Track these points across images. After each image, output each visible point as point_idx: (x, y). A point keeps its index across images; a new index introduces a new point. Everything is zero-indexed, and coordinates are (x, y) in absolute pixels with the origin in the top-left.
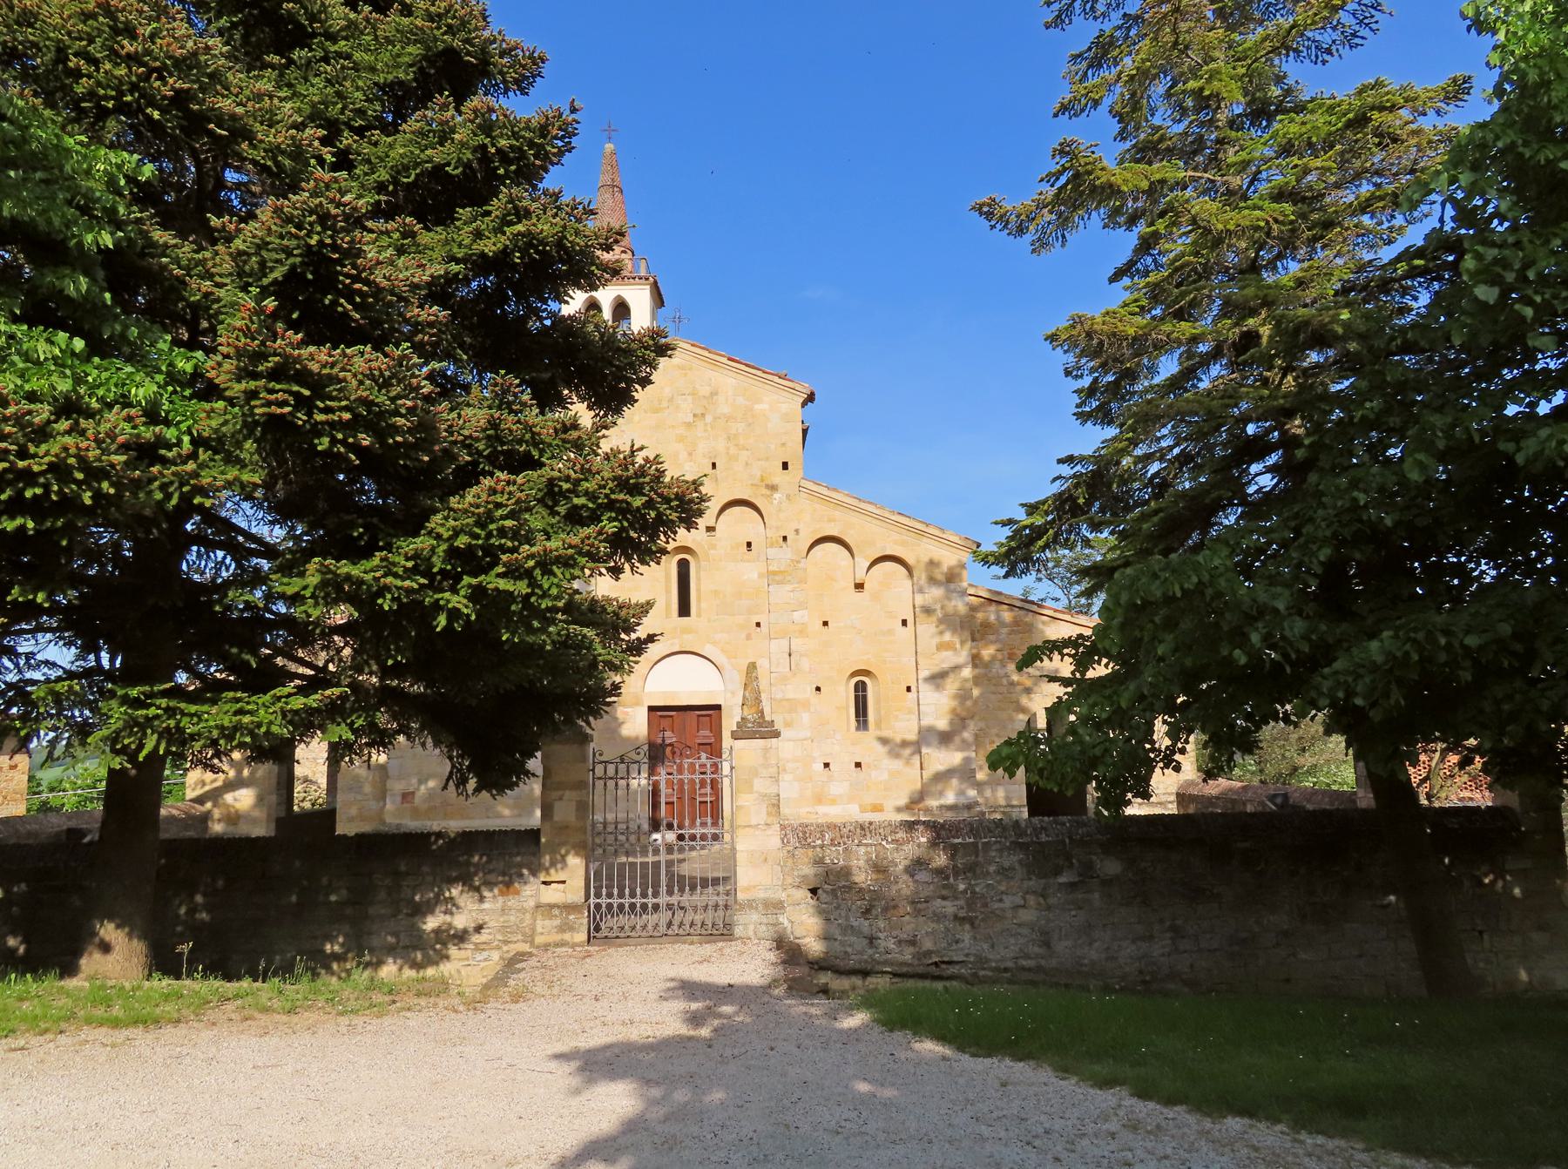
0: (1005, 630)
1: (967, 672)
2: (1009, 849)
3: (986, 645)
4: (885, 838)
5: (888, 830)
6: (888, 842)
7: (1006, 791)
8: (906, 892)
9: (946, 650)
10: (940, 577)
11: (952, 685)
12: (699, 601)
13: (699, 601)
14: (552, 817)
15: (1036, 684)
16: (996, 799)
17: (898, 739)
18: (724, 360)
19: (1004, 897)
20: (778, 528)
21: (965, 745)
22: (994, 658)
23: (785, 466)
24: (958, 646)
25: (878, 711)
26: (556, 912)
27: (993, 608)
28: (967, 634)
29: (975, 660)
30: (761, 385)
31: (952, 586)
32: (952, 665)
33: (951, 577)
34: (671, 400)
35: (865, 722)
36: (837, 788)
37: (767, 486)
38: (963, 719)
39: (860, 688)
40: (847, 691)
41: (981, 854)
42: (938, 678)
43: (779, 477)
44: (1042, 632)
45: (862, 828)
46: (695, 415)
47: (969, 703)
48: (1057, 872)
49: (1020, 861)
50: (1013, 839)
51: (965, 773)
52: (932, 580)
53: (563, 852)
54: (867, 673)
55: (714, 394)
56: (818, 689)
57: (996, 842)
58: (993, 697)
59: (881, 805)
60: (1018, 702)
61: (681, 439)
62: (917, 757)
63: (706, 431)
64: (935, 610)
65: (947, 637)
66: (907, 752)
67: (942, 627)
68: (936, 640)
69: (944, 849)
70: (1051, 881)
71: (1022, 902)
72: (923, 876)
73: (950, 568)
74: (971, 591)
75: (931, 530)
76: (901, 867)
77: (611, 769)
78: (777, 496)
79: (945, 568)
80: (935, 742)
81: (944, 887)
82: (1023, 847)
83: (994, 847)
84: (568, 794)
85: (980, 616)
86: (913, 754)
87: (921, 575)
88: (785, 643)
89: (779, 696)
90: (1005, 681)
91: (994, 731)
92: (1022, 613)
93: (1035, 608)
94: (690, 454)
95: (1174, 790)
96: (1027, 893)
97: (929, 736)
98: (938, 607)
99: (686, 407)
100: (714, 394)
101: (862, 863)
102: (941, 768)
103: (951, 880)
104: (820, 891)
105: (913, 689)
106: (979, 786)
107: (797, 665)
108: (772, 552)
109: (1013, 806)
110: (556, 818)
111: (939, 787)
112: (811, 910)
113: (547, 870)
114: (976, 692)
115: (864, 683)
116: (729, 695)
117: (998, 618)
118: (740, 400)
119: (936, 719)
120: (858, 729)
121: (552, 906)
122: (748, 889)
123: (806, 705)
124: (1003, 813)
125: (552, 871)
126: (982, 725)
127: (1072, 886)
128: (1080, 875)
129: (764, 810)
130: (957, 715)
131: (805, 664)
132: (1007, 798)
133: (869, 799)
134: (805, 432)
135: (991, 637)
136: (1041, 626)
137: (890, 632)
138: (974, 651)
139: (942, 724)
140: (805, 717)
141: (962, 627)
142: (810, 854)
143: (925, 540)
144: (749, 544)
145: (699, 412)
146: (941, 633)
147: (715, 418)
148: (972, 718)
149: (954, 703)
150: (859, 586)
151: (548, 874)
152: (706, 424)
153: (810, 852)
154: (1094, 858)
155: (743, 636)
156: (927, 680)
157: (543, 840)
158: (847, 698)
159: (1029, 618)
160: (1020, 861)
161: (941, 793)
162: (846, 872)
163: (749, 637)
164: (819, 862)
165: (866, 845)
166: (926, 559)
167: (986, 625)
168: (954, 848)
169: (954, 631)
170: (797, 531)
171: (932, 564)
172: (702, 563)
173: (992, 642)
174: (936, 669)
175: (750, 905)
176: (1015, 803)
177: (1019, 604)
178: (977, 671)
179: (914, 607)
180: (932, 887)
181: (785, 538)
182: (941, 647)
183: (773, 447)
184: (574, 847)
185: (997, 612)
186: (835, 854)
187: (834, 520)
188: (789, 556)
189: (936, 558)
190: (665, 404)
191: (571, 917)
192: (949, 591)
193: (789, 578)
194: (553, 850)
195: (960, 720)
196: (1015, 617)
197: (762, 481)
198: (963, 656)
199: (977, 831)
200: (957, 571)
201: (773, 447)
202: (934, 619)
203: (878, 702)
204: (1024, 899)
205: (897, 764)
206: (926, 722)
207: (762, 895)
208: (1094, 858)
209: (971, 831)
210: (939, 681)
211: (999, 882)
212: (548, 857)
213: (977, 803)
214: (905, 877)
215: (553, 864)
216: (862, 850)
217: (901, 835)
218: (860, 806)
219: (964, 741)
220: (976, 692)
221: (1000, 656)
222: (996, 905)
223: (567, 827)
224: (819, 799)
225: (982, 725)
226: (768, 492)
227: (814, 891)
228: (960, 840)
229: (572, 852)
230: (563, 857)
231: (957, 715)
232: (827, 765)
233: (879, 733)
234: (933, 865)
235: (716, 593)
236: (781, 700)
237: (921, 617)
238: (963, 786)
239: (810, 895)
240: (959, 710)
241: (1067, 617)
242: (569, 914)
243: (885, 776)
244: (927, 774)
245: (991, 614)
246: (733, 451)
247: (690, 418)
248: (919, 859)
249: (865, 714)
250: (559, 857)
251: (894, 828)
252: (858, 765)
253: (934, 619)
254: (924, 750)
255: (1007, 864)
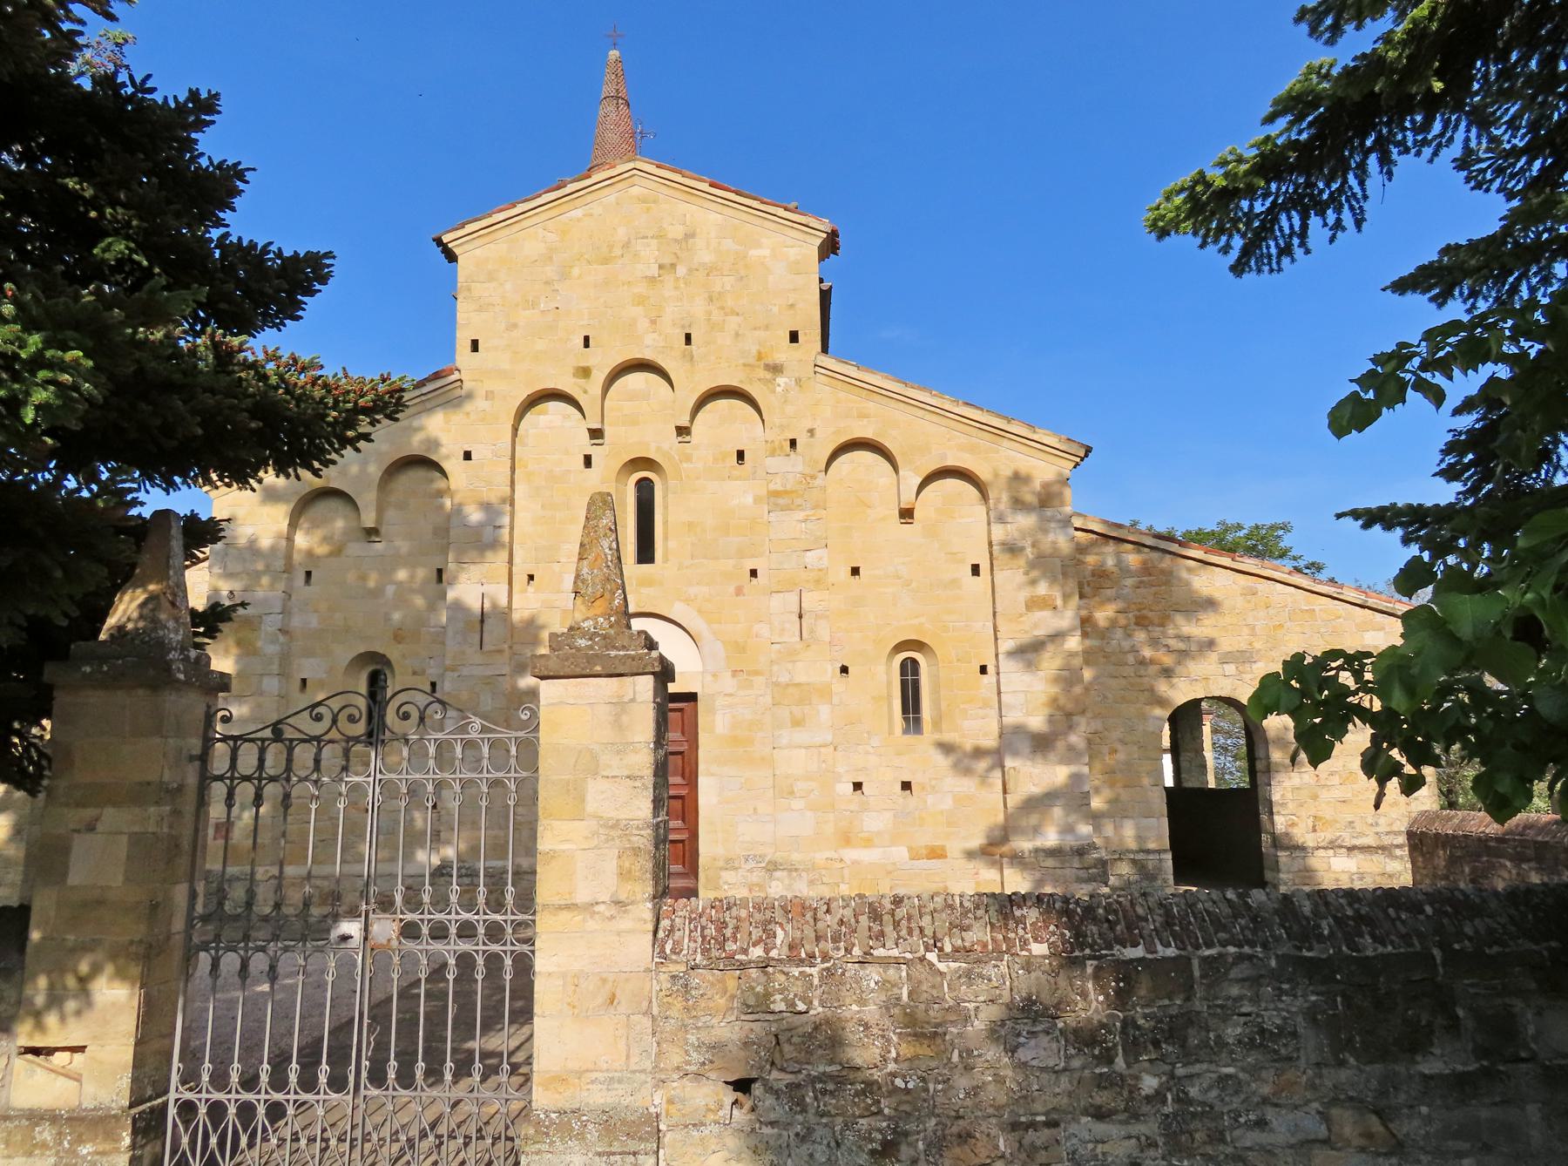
0: (1129, 582)
1: (1074, 643)
2: (1276, 976)
3: (1102, 603)
4: (936, 944)
5: (944, 919)
6: (943, 956)
7: (1138, 828)
8: (994, 1094)
9: (1041, 609)
10: (1029, 498)
11: (1050, 663)
12: (666, 538)
13: (666, 538)
14: (65, 875)
15: (1179, 663)
16: (1121, 839)
17: (968, 746)
18: (705, 186)
19: (1270, 1113)
20: (782, 428)
21: (1072, 755)
22: (1113, 623)
23: (794, 337)
24: (1059, 602)
25: (936, 703)
26: (45, 1133)
27: (1110, 548)
28: (1072, 585)
29: (1086, 625)
30: (759, 221)
31: (1049, 512)
32: (1050, 631)
33: (1047, 499)
34: (627, 245)
35: (918, 721)
36: (875, 822)
37: (768, 367)
38: (1069, 715)
39: (910, 670)
40: (888, 673)
41: (1199, 992)
42: (1029, 652)
43: (784, 353)
44: (1188, 584)
45: (876, 915)
46: (661, 267)
47: (1078, 690)
48: (1415, 1043)
49: (1311, 1015)
50: (1286, 949)
51: (1074, 797)
52: (1018, 504)
53: (84, 968)
54: (918, 645)
55: (690, 236)
56: (844, 670)
57: (1240, 958)
58: (1114, 683)
59: (943, 848)
60: (1152, 690)
61: (640, 300)
62: (997, 774)
63: (676, 288)
64: (1022, 549)
65: (1042, 589)
66: (982, 765)
67: (1035, 574)
68: (1024, 595)
69: (1096, 976)
70: (1400, 1068)
71: (1322, 1132)
72: (1041, 1051)
73: (1046, 486)
74: (1077, 523)
75: (1015, 428)
76: (979, 1025)
77: (248, 760)
78: (781, 380)
79: (1037, 485)
80: (1025, 747)
81: (1102, 1082)
82: (1316, 971)
83: (1234, 973)
84: (111, 817)
85: (1091, 559)
86: (991, 769)
87: (1000, 497)
88: (793, 598)
89: (784, 679)
90: (1131, 659)
91: (1116, 734)
92: (1155, 555)
93: (1175, 548)
94: (653, 322)
95: (1403, 826)
96: (1335, 1101)
97: (1015, 740)
98: (1027, 543)
99: (649, 256)
100: (690, 236)
101: (871, 1012)
102: (1036, 790)
103: (1120, 1063)
104: (757, 1089)
105: (991, 669)
106: (1095, 818)
107: (812, 631)
108: (774, 463)
109: (1148, 852)
110: (74, 879)
111: (1034, 819)
112: (732, 1142)
113: (38, 1015)
114: (1088, 674)
115: (914, 662)
116: (709, 678)
117: (1119, 563)
118: (728, 244)
119: (1028, 714)
120: (906, 731)
121: (35, 1117)
122: (560, 1079)
123: (825, 693)
124: (1134, 861)
125: (51, 1020)
126: (1097, 725)
127: (1461, 1086)
128: (1481, 1052)
129: (611, 865)
130: (1059, 708)
131: (824, 631)
132: (1140, 838)
133: (925, 839)
134: (825, 296)
135: (1109, 592)
136: (1184, 575)
137: (955, 583)
138: (1084, 613)
139: (1037, 722)
140: (824, 711)
141: (1064, 574)
142: (732, 984)
143: (1006, 443)
144: (741, 455)
145: (667, 260)
146: (1033, 582)
147: (690, 271)
148: (1083, 712)
149: (1054, 690)
150: (907, 514)
151: (40, 1026)
152: (677, 279)
153: (731, 980)
154: (1518, 1005)
155: (732, 589)
156: (1012, 654)
157: (35, 935)
158: (889, 684)
159: (1167, 562)
160: (1311, 1015)
161: (1036, 830)
162: (828, 1037)
163: (739, 591)
164: (757, 1006)
165: (885, 962)
166: (1009, 473)
167: (1101, 574)
168: (1126, 971)
169: (1053, 580)
170: (811, 432)
171: (1018, 478)
172: (672, 483)
173: (1109, 600)
174: (1025, 638)
175: (567, 1123)
176: (1152, 846)
177: (1149, 541)
178: (1088, 642)
179: (990, 544)
180: (1065, 1082)
181: (793, 443)
182: (1033, 604)
183: (775, 309)
184: (113, 957)
185: (1118, 554)
186: (797, 988)
187: (867, 416)
188: (800, 468)
189: (1023, 470)
190: (617, 251)
191: (86, 1150)
192: (1044, 520)
193: (799, 501)
194: (60, 959)
195: (1063, 717)
196: (1144, 563)
197: (760, 357)
198: (1067, 618)
199: (1185, 928)
200: (1056, 488)
201: (775, 309)
202: (1022, 562)
203: (936, 690)
204: (1325, 1117)
205: (967, 785)
206: (1011, 718)
207: (597, 1097)
208: (1518, 1005)
209: (1168, 924)
210: (1029, 656)
211: (1254, 1071)
212: (42, 982)
213: (1093, 846)
214: (992, 1053)
215: (55, 1000)
216: (873, 974)
217: (978, 934)
218: (910, 849)
219: (1071, 748)
220: (1088, 674)
221: (1122, 621)
222: (1251, 1138)
223: (100, 902)
224: (847, 839)
225: (1097, 725)
226: (769, 376)
227: (742, 1086)
228: (1138, 952)
229: (109, 969)
230: (83, 981)
231: (1059, 708)
232: (858, 786)
233: (937, 736)
234: (1069, 1020)
235: (690, 525)
236: (788, 685)
237: (1002, 558)
238: (1072, 818)
239: (729, 1096)
240: (1062, 701)
241: (1226, 561)
242: (80, 1140)
243: (948, 803)
244: (1013, 800)
245: (1108, 557)
246: (717, 316)
247: (654, 271)
248: (1029, 1002)
249: (917, 708)
250: (71, 982)
251: (959, 913)
252: (906, 786)
253: (1022, 562)
254: (1009, 762)
255: (1272, 1020)
